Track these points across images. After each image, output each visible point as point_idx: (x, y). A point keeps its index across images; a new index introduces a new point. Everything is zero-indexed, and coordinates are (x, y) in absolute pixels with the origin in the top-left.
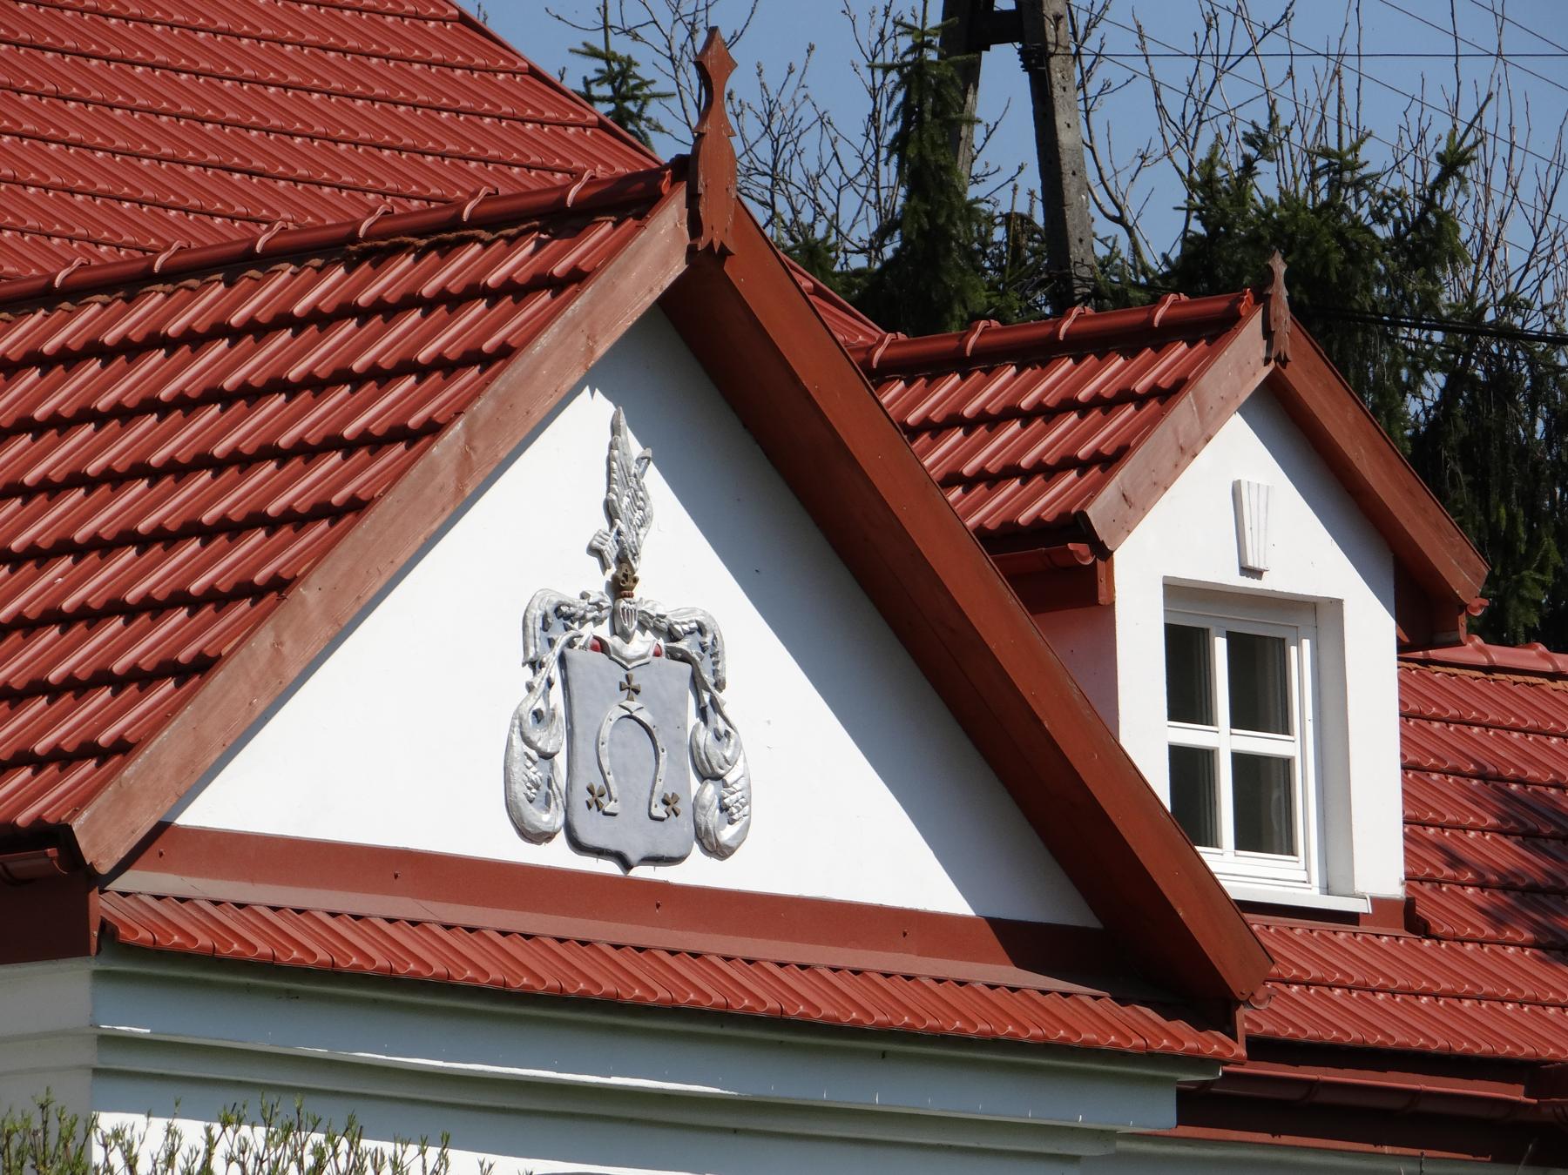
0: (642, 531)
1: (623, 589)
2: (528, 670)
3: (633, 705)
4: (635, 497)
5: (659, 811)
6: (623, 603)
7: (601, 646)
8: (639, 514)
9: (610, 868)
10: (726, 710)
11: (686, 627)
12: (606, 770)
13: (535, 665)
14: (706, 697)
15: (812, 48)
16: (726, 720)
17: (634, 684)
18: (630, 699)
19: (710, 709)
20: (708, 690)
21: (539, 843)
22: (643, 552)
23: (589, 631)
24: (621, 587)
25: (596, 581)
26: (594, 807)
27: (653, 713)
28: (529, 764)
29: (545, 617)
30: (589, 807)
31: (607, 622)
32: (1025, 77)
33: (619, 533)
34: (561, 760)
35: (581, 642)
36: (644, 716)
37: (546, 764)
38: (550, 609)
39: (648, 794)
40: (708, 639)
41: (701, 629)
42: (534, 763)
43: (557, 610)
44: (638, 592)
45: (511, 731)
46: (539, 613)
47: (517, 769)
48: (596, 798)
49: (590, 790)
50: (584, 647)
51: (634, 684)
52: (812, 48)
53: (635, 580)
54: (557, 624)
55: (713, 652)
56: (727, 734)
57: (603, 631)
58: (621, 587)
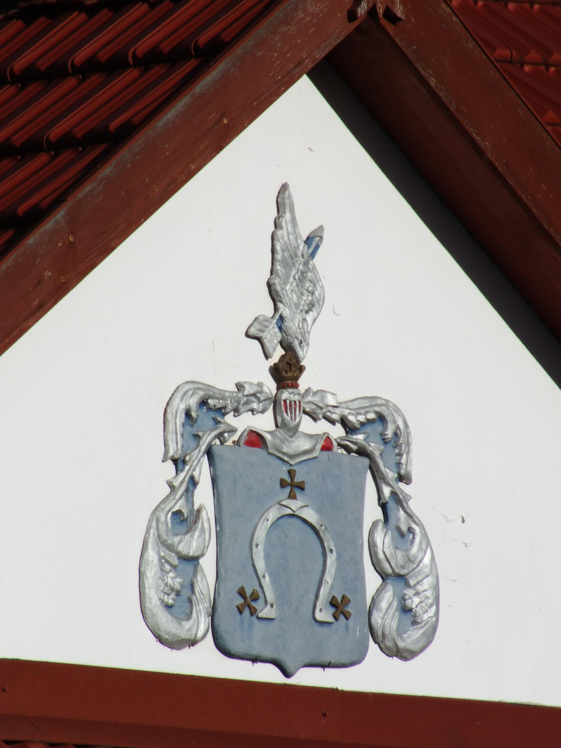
0: (310, 317)
1: (285, 379)
2: (170, 466)
3: (294, 505)
4: (302, 279)
5: (324, 614)
6: (285, 395)
7: (255, 439)
8: (306, 298)
9: (268, 674)
10: (412, 505)
11: (362, 418)
12: (260, 573)
13: (178, 463)
14: (387, 491)
15: (463, 521)
16: (410, 515)
17: (298, 479)
18: (292, 496)
19: (391, 505)
20: (388, 484)
21: (179, 649)
22: (313, 338)
23: (242, 423)
24: (287, 371)
25: (258, 372)
26: (247, 612)
27: (320, 511)
28: (168, 567)
29: (188, 414)
30: (241, 612)
31: (270, 412)
32: (174, 466)
33: (281, 318)
34: (208, 564)
35: (231, 440)
36: (310, 515)
37: (189, 568)
38: (193, 402)
39: (312, 597)
40: (389, 433)
41: (381, 418)
42: (174, 567)
43: (203, 403)
44: (304, 382)
45: (148, 532)
46: (183, 406)
47: (152, 573)
48: (248, 602)
49: (242, 593)
50: (237, 443)
51: (298, 479)
52: (463, 521)
53: (301, 369)
54: (205, 419)
55: (396, 442)
56: (410, 530)
57: (264, 423)
58: (287, 371)
